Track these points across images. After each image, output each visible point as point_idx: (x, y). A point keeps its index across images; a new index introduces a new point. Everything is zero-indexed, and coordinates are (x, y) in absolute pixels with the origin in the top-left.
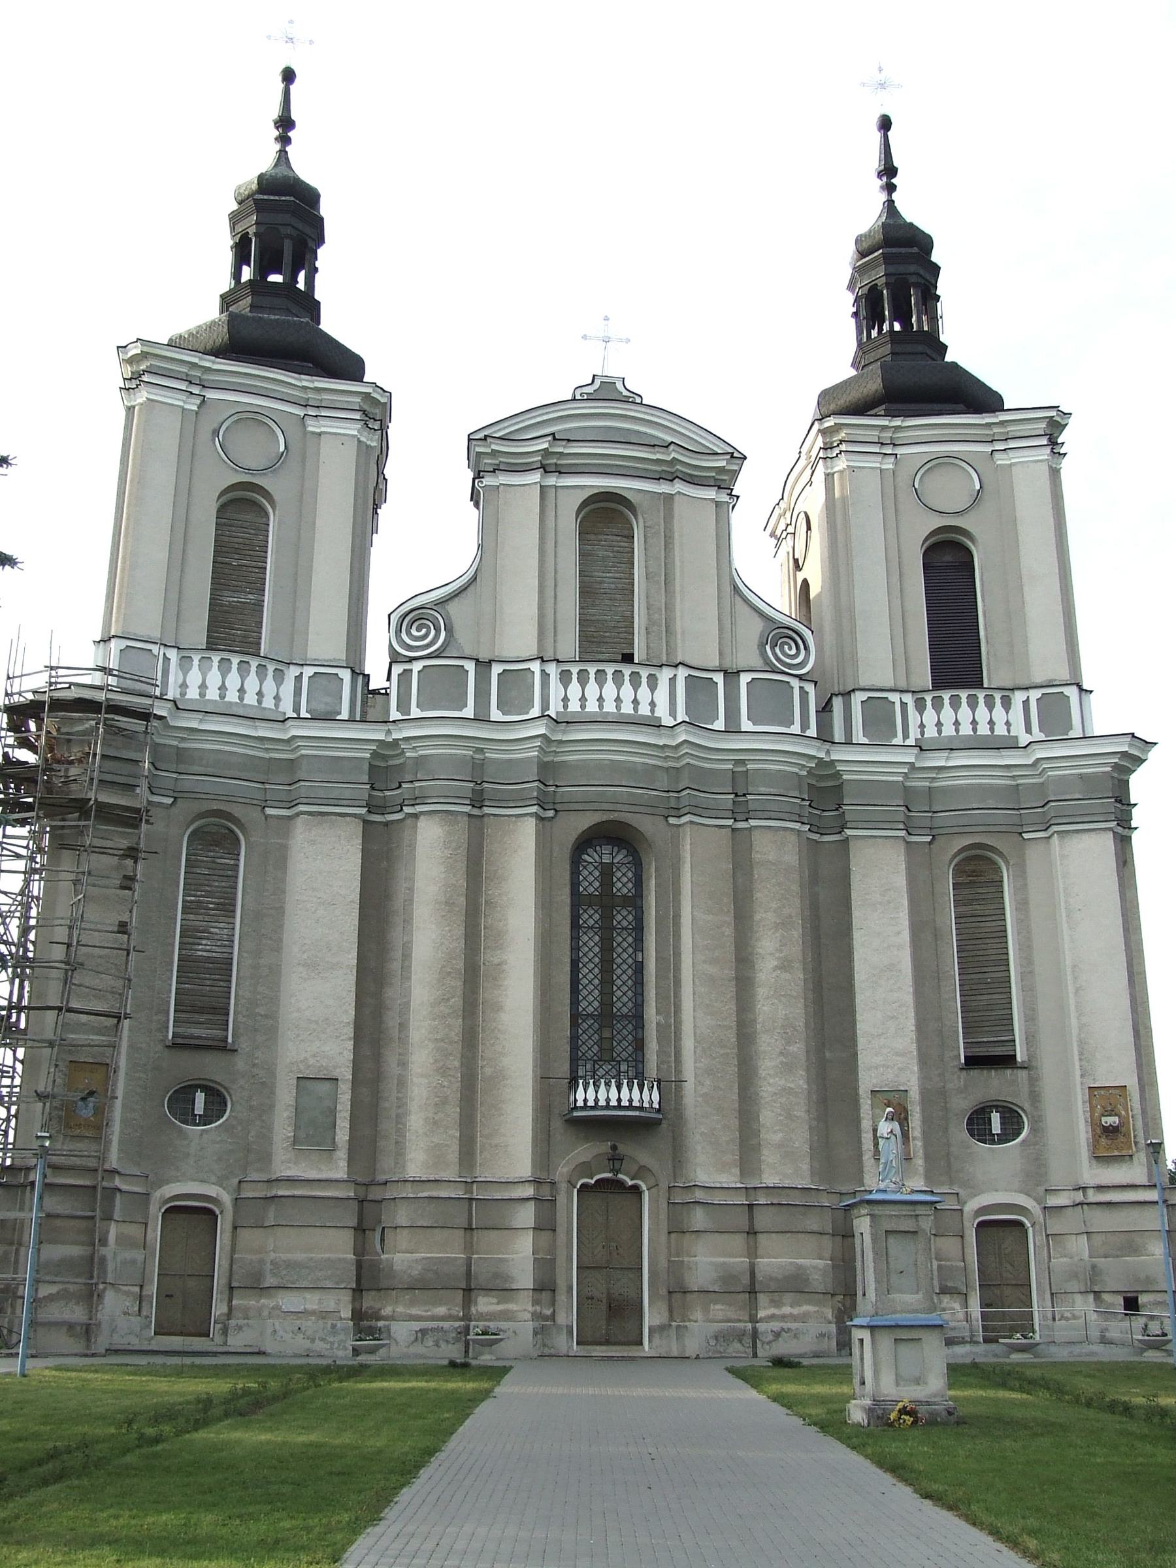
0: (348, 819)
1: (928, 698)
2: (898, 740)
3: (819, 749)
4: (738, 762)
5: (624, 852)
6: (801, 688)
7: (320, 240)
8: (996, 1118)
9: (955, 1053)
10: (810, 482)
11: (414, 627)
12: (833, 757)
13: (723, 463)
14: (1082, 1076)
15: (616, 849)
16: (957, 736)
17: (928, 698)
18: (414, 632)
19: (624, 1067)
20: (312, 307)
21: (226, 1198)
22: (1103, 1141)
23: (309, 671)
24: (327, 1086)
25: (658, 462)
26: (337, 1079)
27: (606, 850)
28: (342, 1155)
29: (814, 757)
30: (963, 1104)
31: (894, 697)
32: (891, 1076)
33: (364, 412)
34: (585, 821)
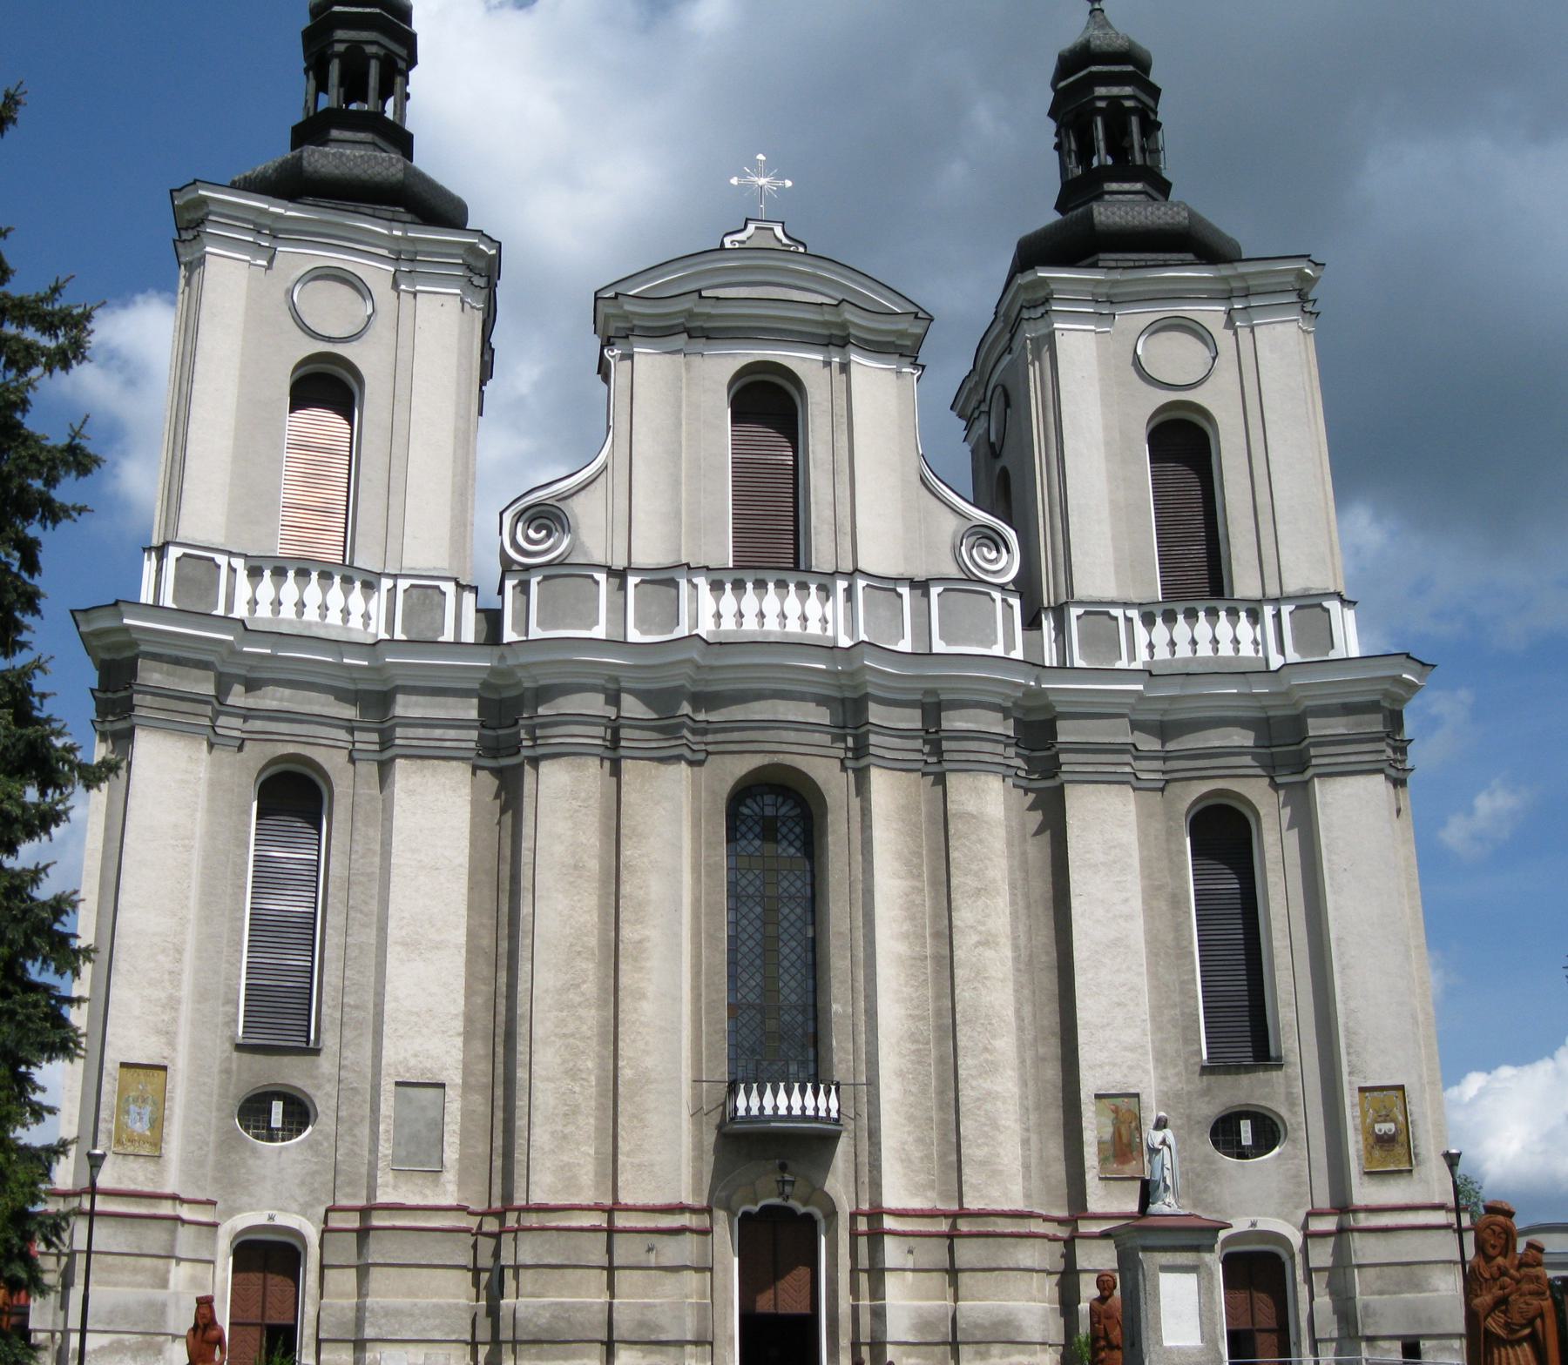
0: (454, 763)
1: (1158, 610)
2: (1122, 664)
3: (1026, 676)
4: (927, 692)
5: (798, 811)
6: (1004, 600)
7: (412, 61)
8: (1246, 1128)
9: (1196, 1047)
10: (1009, 350)
11: (534, 525)
12: (510, 662)
13: (687, 306)
14: (1350, 1073)
15: (780, 800)
16: (1217, 659)
17: (1158, 610)
18: (531, 533)
19: (793, 1068)
20: (402, 141)
21: (312, 1233)
22: (1377, 1153)
23: (403, 584)
24: (431, 1092)
25: (825, 324)
26: (442, 1086)
27: (768, 799)
28: (450, 1176)
29: (1018, 685)
30: (1210, 1110)
31: (1115, 612)
32: (1118, 1077)
33: (469, 267)
34: (741, 766)
